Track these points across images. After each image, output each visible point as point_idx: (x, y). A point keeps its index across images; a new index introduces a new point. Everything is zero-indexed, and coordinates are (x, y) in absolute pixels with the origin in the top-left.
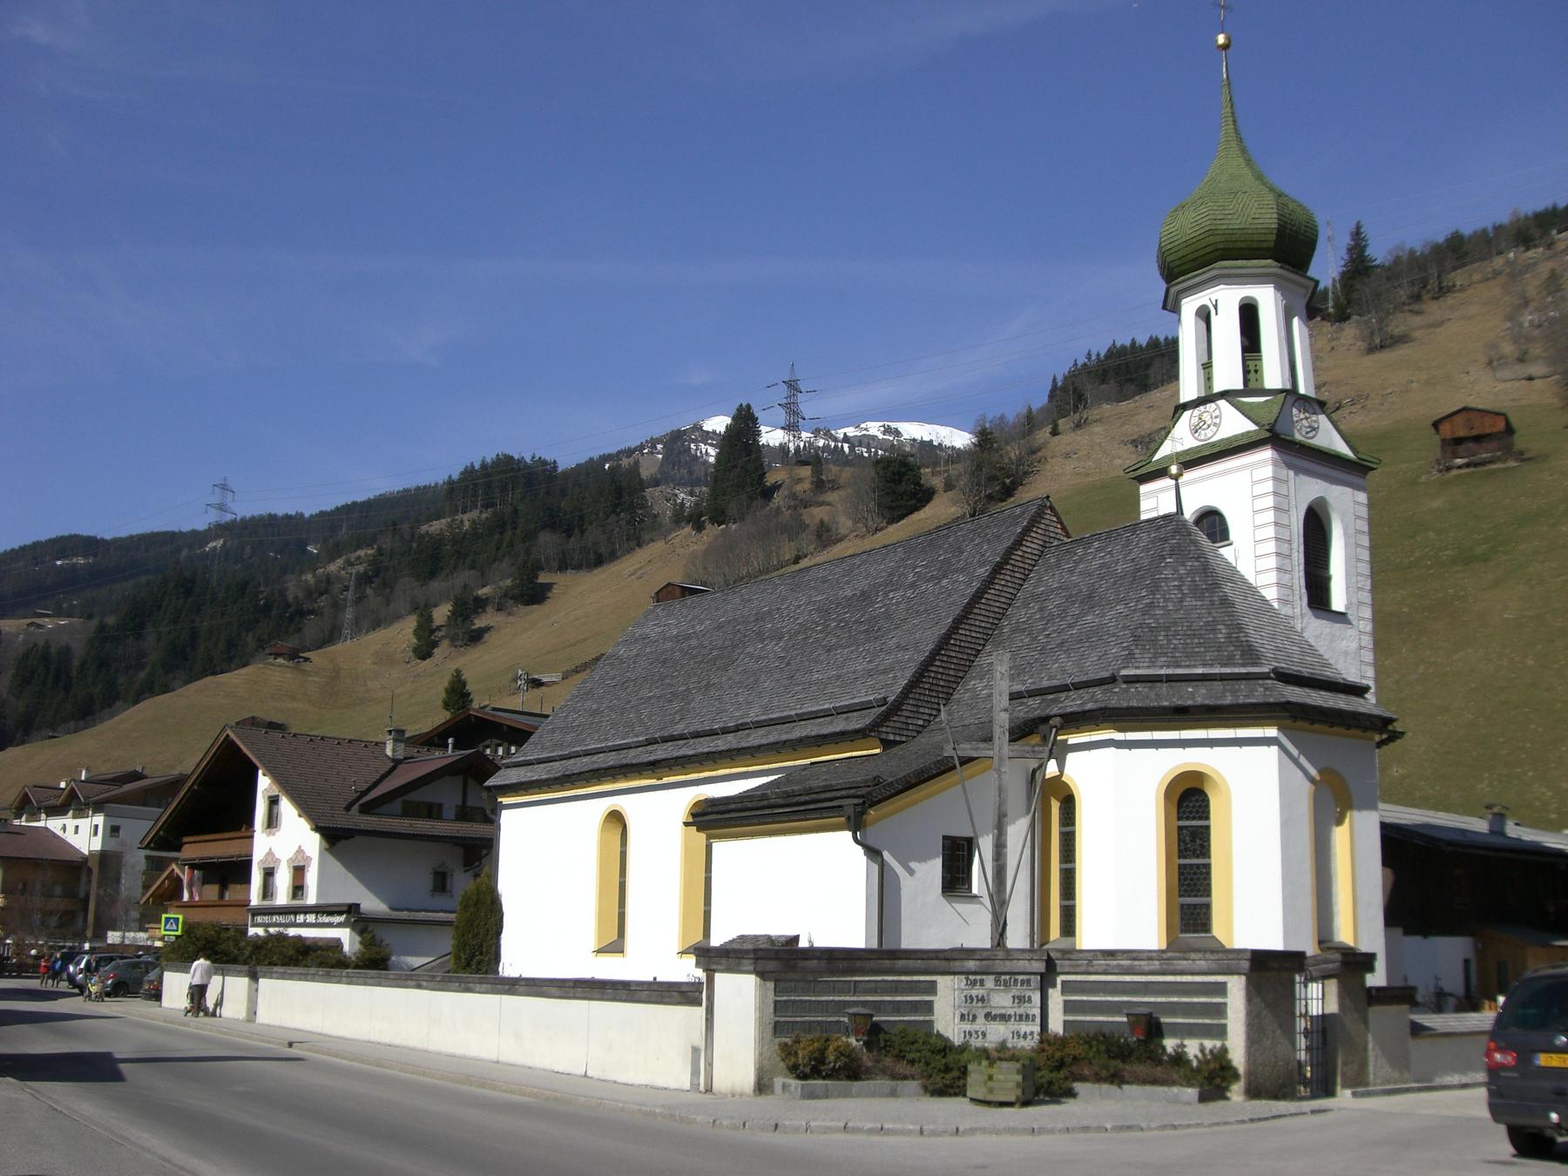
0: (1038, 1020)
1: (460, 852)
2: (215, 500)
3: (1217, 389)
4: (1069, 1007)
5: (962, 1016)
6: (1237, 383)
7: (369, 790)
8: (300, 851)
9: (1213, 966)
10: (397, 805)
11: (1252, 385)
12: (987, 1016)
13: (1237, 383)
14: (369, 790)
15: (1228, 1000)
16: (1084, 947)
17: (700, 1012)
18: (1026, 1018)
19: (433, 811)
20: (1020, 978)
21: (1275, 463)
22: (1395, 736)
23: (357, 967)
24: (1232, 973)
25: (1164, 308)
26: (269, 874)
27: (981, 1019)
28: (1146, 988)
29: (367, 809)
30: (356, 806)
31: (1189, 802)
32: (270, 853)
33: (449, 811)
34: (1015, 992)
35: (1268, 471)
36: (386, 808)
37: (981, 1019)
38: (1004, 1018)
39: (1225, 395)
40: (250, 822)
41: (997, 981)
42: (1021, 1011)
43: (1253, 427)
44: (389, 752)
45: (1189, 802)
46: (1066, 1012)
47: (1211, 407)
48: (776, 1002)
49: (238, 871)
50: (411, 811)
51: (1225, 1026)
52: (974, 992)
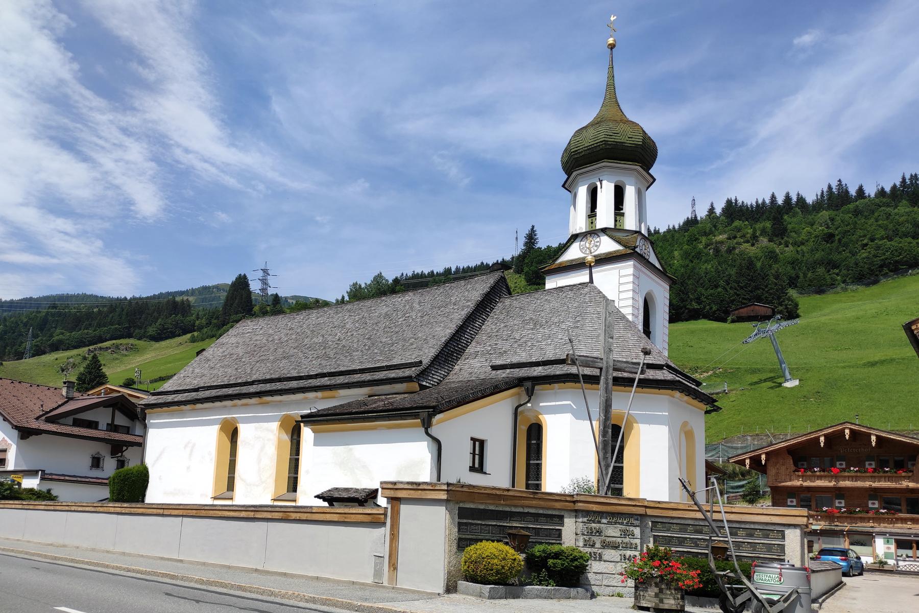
1: (109, 446)
7: (51, 411)
10: (70, 420)
11: (618, 227)
14: (51, 411)
15: (786, 543)
17: (386, 531)
19: (93, 425)
21: (635, 266)
22: (717, 409)
23: (373, 296)
25: (563, 186)
29: (52, 420)
30: (44, 418)
31: (478, 467)
33: (103, 425)
35: (631, 271)
36: (61, 421)
38: (616, 547)
39: (604, 231)
43: (621, 248)
44: (64, 393)
48: (459, 523)
50: (78, 423)
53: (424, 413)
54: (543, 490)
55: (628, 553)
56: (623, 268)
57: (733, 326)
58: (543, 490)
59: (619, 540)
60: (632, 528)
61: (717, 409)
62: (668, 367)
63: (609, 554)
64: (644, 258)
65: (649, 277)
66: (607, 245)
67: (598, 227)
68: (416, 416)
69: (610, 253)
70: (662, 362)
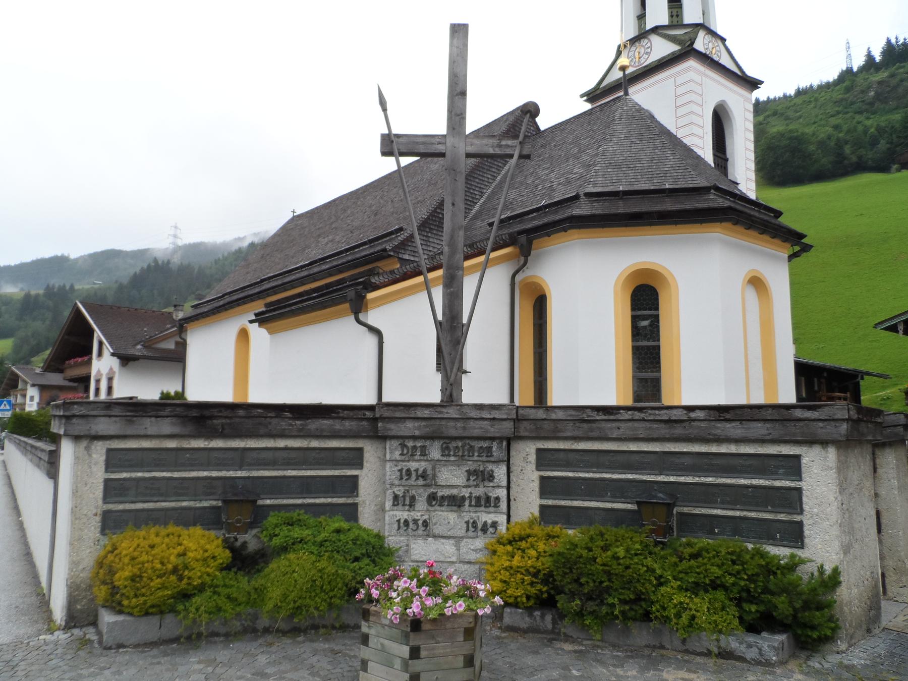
0: (503, 506)
2: (172, 232)
3: (648, 27)
4: (547, 487)
5: (396, 497)
6: (664, 20)
8: (111, 369)
9: (776, 434)
12: (432, 499)
13: (664, 20)
15: (804, 485)
16: (554, 404)
18: (488, 502)
20: (477, 444)
22: (807, 248)
24: (811, 442)
26: (98, 381)
27: (421, 504)
28: (665, 462)
31: (645, 300)
32: (99, 371)
34: (471, 465)
37: (421, 504)
38: (456, 502)
39: (656, 30)
40: (90, 352)
41: (445, 450)
42: (479, 491)
45: (645, 300)
46: (543, 493)
47: (644, 42)
49: (85, 381)
51: (800, 524)
52: (413, 465)
53: (351, 293)
54: (666, 401)
55: (486, 517)
56: (679, 74)
57: (899, 175)
58: (666, 401)
59: (465, 493)
60: (490, 467)
61: (807, 248)
62: (717, 189)
63: (448, 520)
64: (712, 60)
65: (731, 90)
66: (661, 48)
67: (648, 28)
68: (342, 300)
69: (659, 60)
70: (705, 184)
